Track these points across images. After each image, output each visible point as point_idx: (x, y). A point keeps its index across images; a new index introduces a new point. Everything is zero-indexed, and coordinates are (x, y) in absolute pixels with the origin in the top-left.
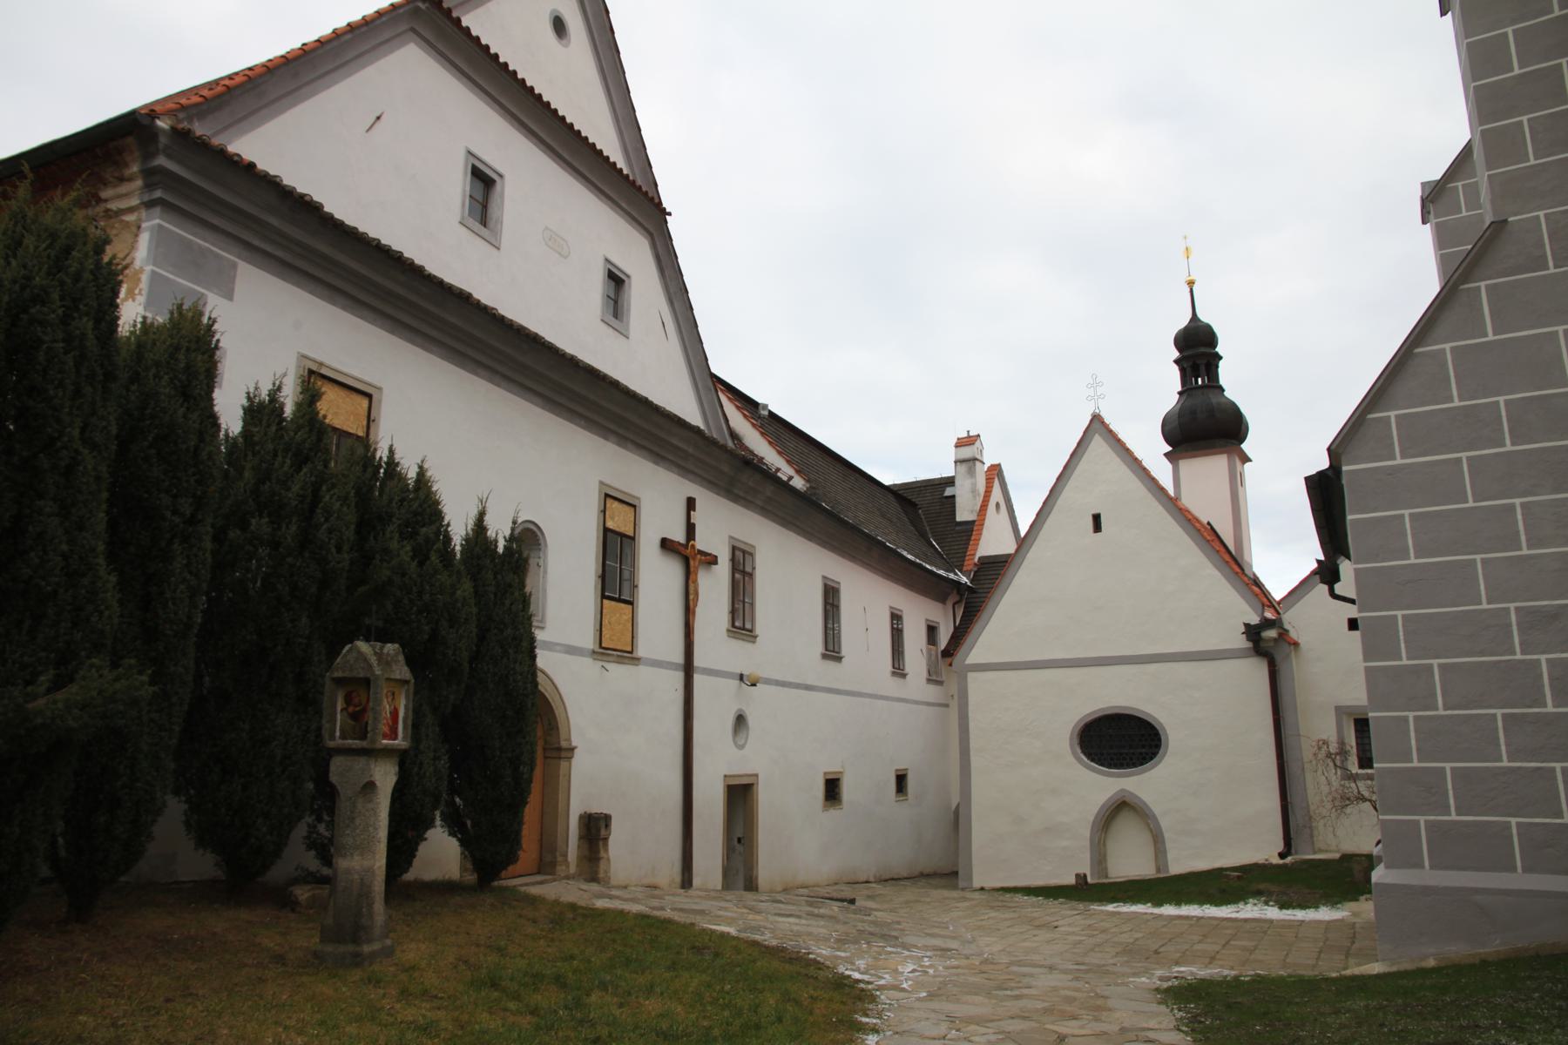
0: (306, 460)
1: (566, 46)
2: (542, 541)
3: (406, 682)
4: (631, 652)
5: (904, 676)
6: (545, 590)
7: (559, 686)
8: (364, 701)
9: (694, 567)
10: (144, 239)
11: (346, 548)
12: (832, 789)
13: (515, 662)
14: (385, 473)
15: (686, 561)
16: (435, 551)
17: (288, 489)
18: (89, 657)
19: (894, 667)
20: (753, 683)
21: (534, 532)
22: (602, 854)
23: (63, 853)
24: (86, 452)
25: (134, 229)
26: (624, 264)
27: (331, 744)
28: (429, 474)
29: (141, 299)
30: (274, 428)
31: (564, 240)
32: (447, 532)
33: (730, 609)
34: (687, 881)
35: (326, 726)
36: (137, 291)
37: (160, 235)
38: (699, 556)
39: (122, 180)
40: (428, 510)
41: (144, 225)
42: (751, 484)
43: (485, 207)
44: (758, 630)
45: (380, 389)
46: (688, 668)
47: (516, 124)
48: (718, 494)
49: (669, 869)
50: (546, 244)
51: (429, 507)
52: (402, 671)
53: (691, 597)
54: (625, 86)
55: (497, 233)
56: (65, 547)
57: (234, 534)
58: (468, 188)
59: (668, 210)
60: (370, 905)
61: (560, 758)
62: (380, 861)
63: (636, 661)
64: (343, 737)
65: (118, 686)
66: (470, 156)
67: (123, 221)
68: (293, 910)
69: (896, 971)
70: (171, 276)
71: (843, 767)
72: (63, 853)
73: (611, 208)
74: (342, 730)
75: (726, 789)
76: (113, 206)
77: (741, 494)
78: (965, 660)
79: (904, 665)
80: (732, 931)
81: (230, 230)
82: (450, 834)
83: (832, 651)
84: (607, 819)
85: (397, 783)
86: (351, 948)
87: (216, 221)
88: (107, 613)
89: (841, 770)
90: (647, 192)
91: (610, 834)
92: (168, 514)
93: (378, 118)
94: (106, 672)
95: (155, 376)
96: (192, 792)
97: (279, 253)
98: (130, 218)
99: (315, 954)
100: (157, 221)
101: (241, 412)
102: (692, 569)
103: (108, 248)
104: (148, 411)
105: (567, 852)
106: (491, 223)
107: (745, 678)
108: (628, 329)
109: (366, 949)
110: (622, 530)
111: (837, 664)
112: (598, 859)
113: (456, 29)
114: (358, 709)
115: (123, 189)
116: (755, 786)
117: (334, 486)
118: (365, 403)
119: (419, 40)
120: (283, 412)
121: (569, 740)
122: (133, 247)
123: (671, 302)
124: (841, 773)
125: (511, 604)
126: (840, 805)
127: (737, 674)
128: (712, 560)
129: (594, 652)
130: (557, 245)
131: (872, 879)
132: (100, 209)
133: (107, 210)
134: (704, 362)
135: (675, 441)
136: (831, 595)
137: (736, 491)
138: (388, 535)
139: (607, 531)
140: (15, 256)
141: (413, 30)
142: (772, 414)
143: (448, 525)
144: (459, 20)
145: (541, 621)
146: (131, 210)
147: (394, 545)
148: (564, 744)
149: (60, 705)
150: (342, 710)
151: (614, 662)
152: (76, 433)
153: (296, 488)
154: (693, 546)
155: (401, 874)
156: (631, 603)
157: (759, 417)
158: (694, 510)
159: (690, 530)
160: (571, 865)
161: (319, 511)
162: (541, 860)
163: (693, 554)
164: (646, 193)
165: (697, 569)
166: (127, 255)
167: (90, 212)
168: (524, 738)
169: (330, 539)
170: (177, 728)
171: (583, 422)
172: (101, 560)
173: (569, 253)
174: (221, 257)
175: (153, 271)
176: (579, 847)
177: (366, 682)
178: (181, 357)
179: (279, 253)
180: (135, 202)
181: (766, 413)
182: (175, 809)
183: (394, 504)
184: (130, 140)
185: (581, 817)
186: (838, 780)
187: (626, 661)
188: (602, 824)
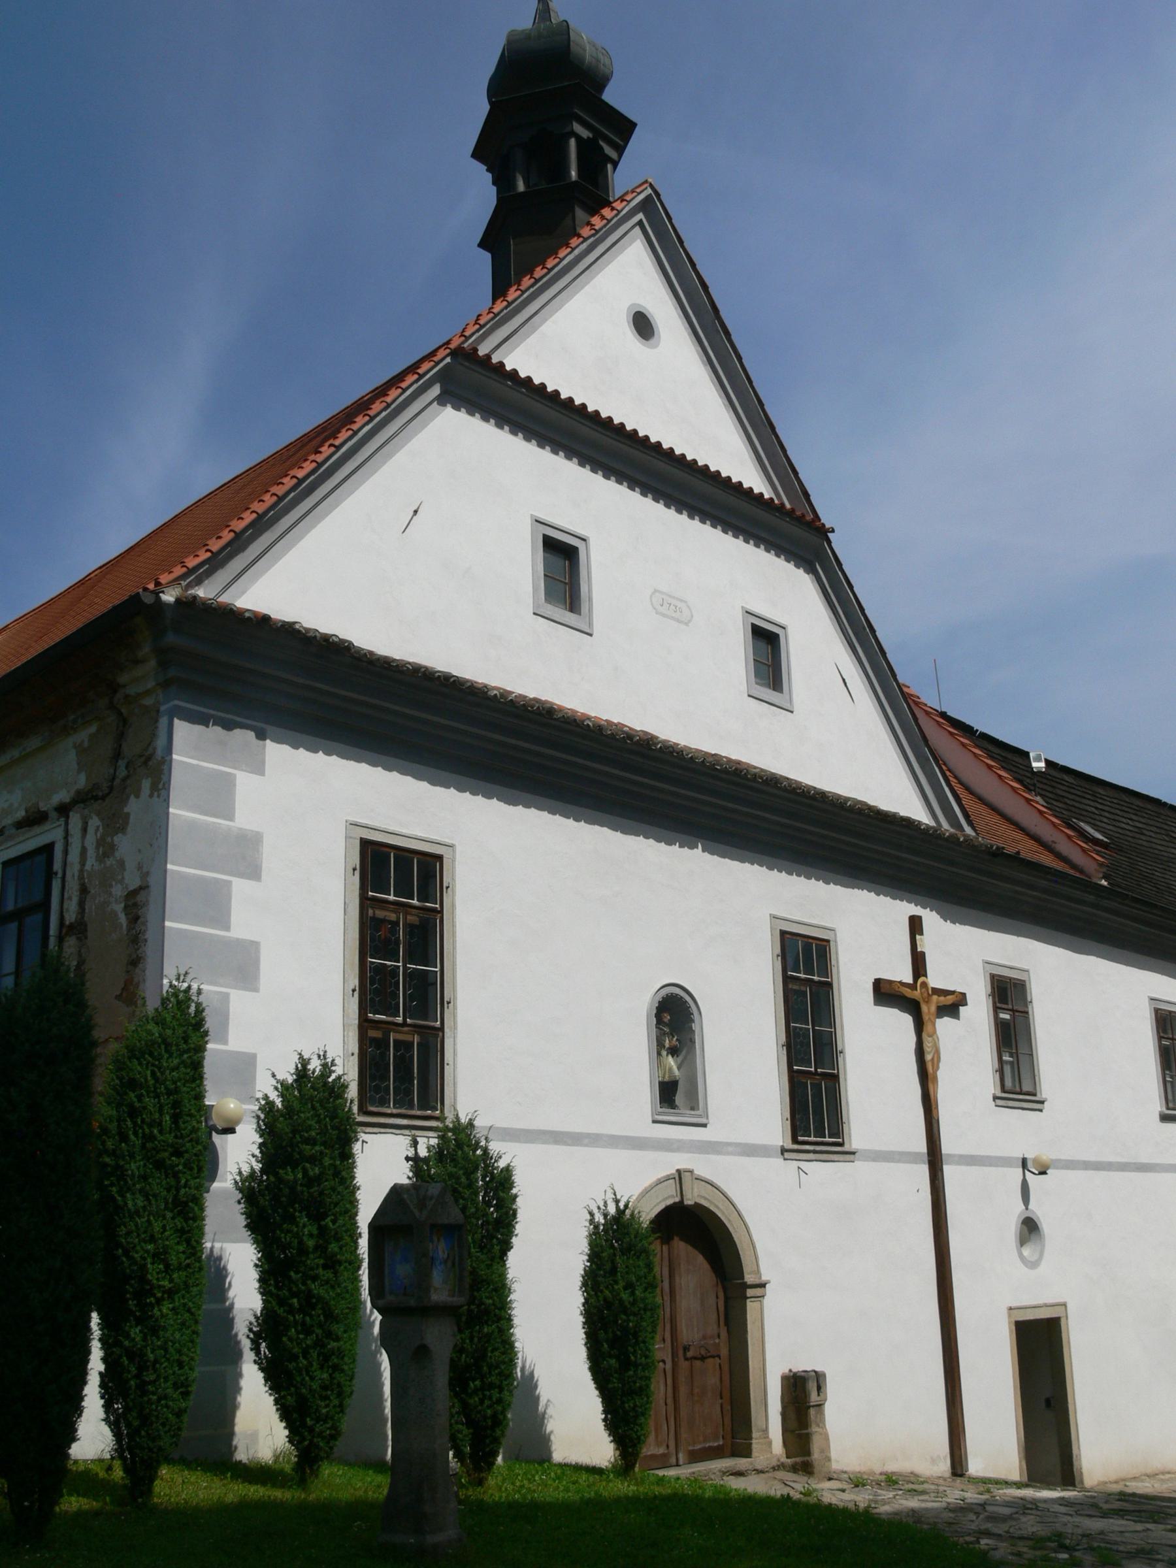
4: (841, 1145)
20: (1043, 1170)
26: (772, 611)
31: (681, 601)
36: (161, 786)
38: (935, 997)
39: (137, 662)
41: (163, 708)
46: (935, 1159)
49: (944, 1467)
59: (827, 526)
75: (1014, 1328)
93: (416, 512)
98: (148, 701)
127: (1018, 1158)
128: (953, 1005)
133: (127, 696)
146: (148, 693)
154: (924, 984)
158: (921, 934)
159: (919, 963)
166: (149, 744)
180: (151, 684)
186: (439, 858)
188: (812, 1386)
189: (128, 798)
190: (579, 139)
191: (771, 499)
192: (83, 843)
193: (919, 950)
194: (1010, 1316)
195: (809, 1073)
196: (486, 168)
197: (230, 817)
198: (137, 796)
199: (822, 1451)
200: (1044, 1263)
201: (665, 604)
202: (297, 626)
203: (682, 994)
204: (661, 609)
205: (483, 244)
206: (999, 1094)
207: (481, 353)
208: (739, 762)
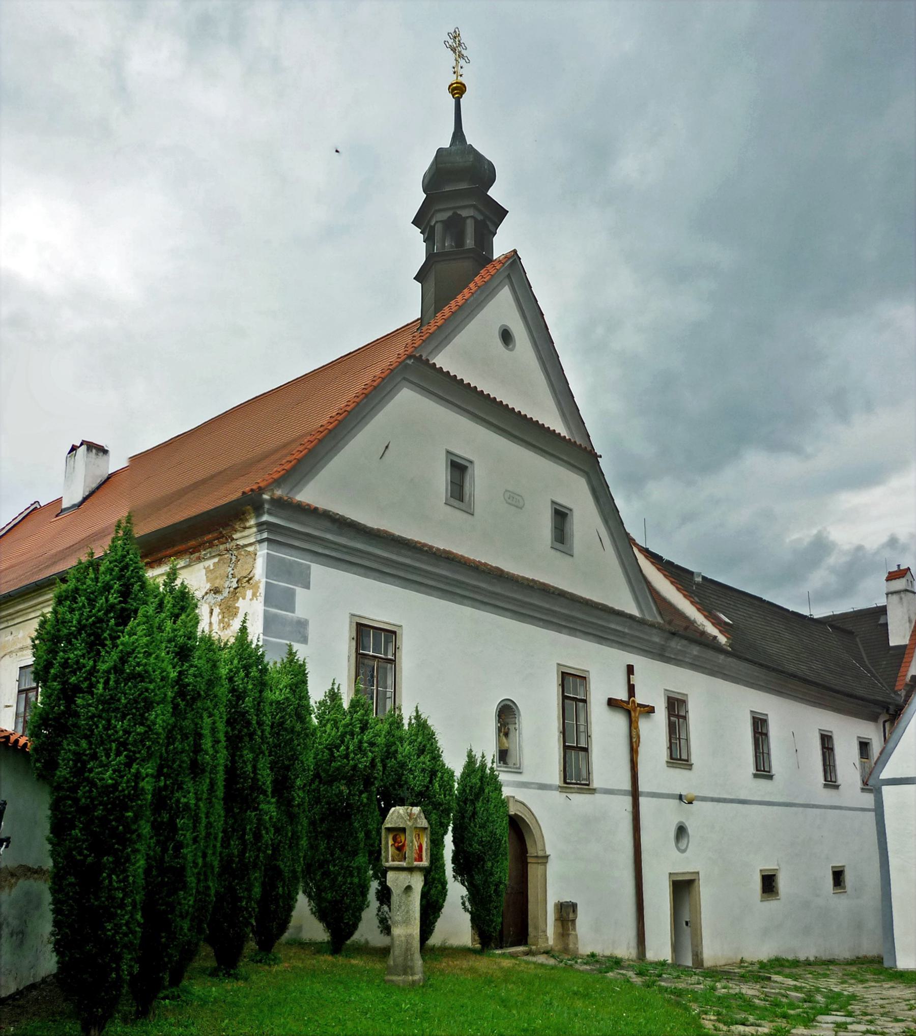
1: (511, 350)
2: (516, 712)
3: (426, 829)
4: (588, 785)
5: (837, 787)
8: (403, 841)
15: (629, 713)
19: (826, 780)
20: (690, 801)
27: (387, 865)
29: (261, 599)
31: (519, 495)
33: (669, 746)
36: (258, 594)
37: (271, 561)
38: (638, 708)
39: (245, 528)
41: (258, 553)
46: (635, 794)
50: (507, 503)
54: (560, 367)
58: (449, 478)
59: (598, 454)
60: (412, 955)
62: (415, 930)
63: (593, 791)
66: (449, 454)
69: (566, 964)
71: (778, 865)
73: (555, 462)
74: (392, 856)
76: (241, 542)
78: (879, 776)
83: (763, 771)
89: (777, 868)
90: (581, 445)
91: (576, 917)
93: (387, 447)
98: (250, 549)
102: (633, 719)
105: (546, 930)
106: (466, 498)
107: (683, 797)
111: (770, 781)
112: (568, 935)
114: (400, 844)
115: (246, 533)
116: (697, 881)
121: (544, 850)
123: (606, 521)
124: (777, 870)
126: (778, 896)
128: (650, 710)
132: (233, 544)
134: (635, 561)
135: (613, 626)
136: (760, 726)
137: (667, 654)
141: (404, 379)
144: (434, 364)
146: (251, 544)
150: (392, 845)
151: (575, 793)
154: (634, 702)
158: (633, 674)
159: (631, 689)
160: (549, 938)
163: (633, 707)
167: (228, 546)
171: (541, 624)
173: (524, 504)
180: (252, 540)
181: (700, 579)
185: (556, 905)
186: (774, 875)
189: (238, 599)
191: (570, 439)
192: (210, 620)
193: (631, 683)
195: (574, 747)
197: (293, 612)
198: (244, 599)
200: (688, 850)
201: (511, 498)
203: (511, 704)
204: (509, 501)
205: (417, 278)
206: (670, 760)
207: (424, 358)
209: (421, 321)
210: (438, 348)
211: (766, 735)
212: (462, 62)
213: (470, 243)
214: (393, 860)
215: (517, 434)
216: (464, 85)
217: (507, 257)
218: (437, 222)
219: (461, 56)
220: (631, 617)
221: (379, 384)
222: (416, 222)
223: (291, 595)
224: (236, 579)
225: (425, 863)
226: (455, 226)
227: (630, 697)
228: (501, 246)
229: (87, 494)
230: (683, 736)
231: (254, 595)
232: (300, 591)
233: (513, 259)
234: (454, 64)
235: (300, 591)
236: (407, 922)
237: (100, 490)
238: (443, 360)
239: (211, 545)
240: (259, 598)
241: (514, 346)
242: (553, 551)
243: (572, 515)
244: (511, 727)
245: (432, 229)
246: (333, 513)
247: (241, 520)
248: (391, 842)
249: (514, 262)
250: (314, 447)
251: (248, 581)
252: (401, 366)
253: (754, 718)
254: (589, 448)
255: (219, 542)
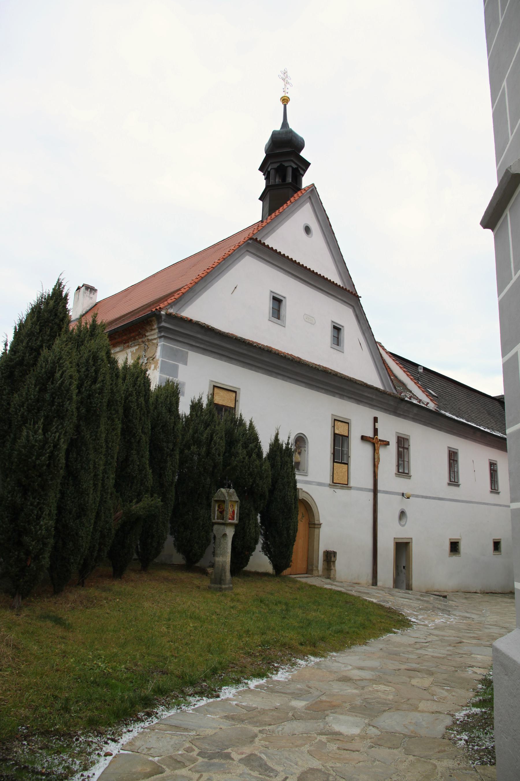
0: (208, 426)
2: (306, 441)
3: (237, 502)
4: (347, 485)
6: (308, 461)
7: (314, 499)
9: (377, 447)
10: (159, 349)
11: (221, 455)
12: (454, 547)
13: (288, 492)
14: (239, 423)
15: (374, 444)
16: (255, 453)
17: (203, 436)
18: (145, 494)
19: (492, 489)
21: (303, 437)
22: (332, 568)
23: (140, 550)
24: (143, 435)
25: (156, 345)
26: (340, 322)
27: (214, 521)
28: (254, 423)
29: (158, 370)
30: (199, 413)
32: (260, 445)
34: (375, 582)
35: (212, 515)
38: (380, 442)
39: (152, 330)
40: (252, 438)
42: (405, 408)
43: (279, 311)
44: (412, 473)
45: (239, 389)
46: (375, 491)
47: (290, 275)
48: (390, 414)
50: (305, 321)
51: (253, 436)
52: (235, 498)
53: (376, 460)
55: (284, 321)
56: (138, 463)
57: (186, 451)
59: (359, 296)
60: (225, 573)
61: (315, 528)
63: (350, 488)
64: (218, 519)
65: (152, 502)
67: (153, 342)
68: (207, 576)
70: (167, 361)
71: (461, 536)
72: (140, 550)
74: (217, 516)
76: (150, 338)
77: (402, 413)
79: (498, 488)
80: (375, 601)
81: (186, 341)
82: (265, 555)
84: (335, 553)
85: (234, 535)
86: (219, 586)
87: (181, 339)
88: (149, 481)
89: (460, 538)
91: (336, 560)
92: (166, 449)
93: (236, 288)
94: (149, 499)
95: (161, 407)
96: (176, 534)
97: (202, 346)
98: (155, 341)
99: (209, 587)
100: (163, 343)
101: (189, 407)
102: (376, 448)
103: (147, 372)
104: (159, 418)
106: (281, 317)
107: (405, 495)
108: (343, 349)
109: (223, 586)
110: (342, 433)
112: (331, 570)
113: (263, 247)
115: (153, 332)
116: (411, 543)
117: (217, 434)
118: (234, 395)
119: (250, 254)
120: (202, 406)
121: (319, 520)
122: (156, 352)
123: (364, 334)
124: (460, 539)
125: (287, 469)
129: (330, 485)
130: (310, 320)
131: (478, 591)
132: (146, 338)
135: (366, 394)
137: (398, 412)
138: (238, 447)
139: (335, 436)
140: (125, 383)
141: (247, 251)
142: (425, 369)
143: (260, 442)
144: (264, 243)
145: (306, 473)
146: (155, 339)
147: (240, 451)
148: (316, 522)
149: (138, 508)
152: (140, 431)
153: (205, 436)
154: (377, 438)
155: (244, 567)
156: (347, 464)
157: (418, 373)
158: (377, 422)
159: (376, 431)
161: (212, 443)
162: (308, 568)
164: (349, 290)
165: (379, 448)
167: (143, 339)
168: (292, 520)
169: (216, 452)
170: (170, 514)
172: (148, 466)
174: (183, 351)
175: (162, 360)
176: (323, 564)
177: (224, 502)
178: (168, 400)
179: (202, 346)
180: (156, 336)
182: (170, 540)
183: (240, 436)
184: (154, 318)
185: (324, 552)
186: (458, 542)
187: (345, 488)
188: (332, 555)
190: (292, 168)
191: (343, 287)
194: (394, 540)
196: (263, 174)
199: (334, 575)
202: (200, 323)
205: (260, 199)
207: (258, 240)
208: (326, 368)
209: (262, 221)
210: (267, 235)
211: (457, 461)
212: (288, 86)
213: (289, 179)
214: (218, 519)
215: (312, 283)
216: (289, 98)
217: (308, 187)
218: (271, 169)
219: (287, 83)
220: (377, 389)
221: (232, 253)
222: (261, 169)
223: (176, 368)
224: (146, 358)
225: (236, 521)
226: (281, 171)
227: (375, 435)
228: (306, 181)
229: (84, 313)
230: (406, 459)
231: (155, 368)
232: (181, 367)
233: (313, 189)
234: (284, 87)
235: (181, 367)
236: (223, 554)
237: (91, 311)
238: (270, 242)
239: (135, 339)
240: (158, 369)
241: (312, 235)
242: (332, 350)
243: (344, 330)
244: (303, 449)
245: (269, 173)
246: (202, 323)
247: (150, 325)
248: (217, 508)
249: (312, 190)
250: (192, 286)
251: (153, 359)
252: (245, 244)
253: (449, 451)
254: (354, 293)
255: (139, 337)
